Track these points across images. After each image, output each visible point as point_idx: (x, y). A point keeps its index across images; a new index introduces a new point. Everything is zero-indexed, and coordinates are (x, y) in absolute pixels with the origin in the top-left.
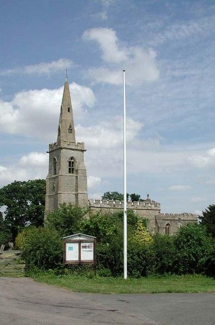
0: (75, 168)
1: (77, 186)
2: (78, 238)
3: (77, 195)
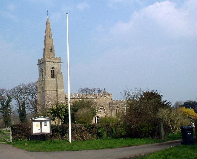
0: (55, 74)
1: (57, 86)
2: (39, 119)
3: (57, 91)
